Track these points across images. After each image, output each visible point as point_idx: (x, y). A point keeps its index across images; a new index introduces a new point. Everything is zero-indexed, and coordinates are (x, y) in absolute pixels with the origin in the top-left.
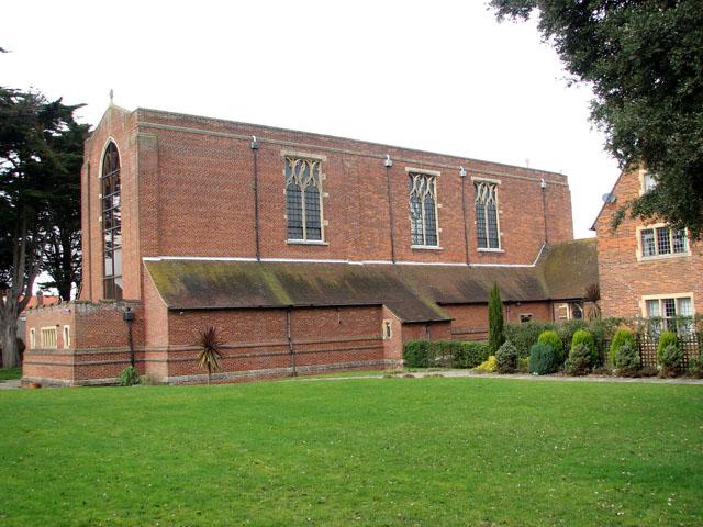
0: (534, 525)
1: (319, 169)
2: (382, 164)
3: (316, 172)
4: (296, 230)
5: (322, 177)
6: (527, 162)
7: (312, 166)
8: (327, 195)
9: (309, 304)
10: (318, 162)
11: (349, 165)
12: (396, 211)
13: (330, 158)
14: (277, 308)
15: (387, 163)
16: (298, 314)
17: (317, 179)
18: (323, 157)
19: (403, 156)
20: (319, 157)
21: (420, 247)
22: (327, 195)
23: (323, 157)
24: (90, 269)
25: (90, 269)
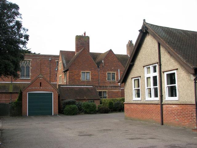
0: (131, 147)
1: (30, 62)
2: (48, 60)
3: (29, 63)
4: (28, 76)
5: (31, 64)
6: (144, 48)
7: (28, 62)
8: (31, 68)
9: (16, 92)
10: (30, 61)
11: (38, 61)
12: (52, 71)
13: (33, 60)
14: (175, 104)
15: (50, 60)
16: (13, 94)
17: (29, 64)
18: (31, 60)
19: (55, 58)
20: (30, 59)
21: (24, 78)
22: (31, 68)
23: (31, 60)
24: (168, 104)
25: (168, 104)
